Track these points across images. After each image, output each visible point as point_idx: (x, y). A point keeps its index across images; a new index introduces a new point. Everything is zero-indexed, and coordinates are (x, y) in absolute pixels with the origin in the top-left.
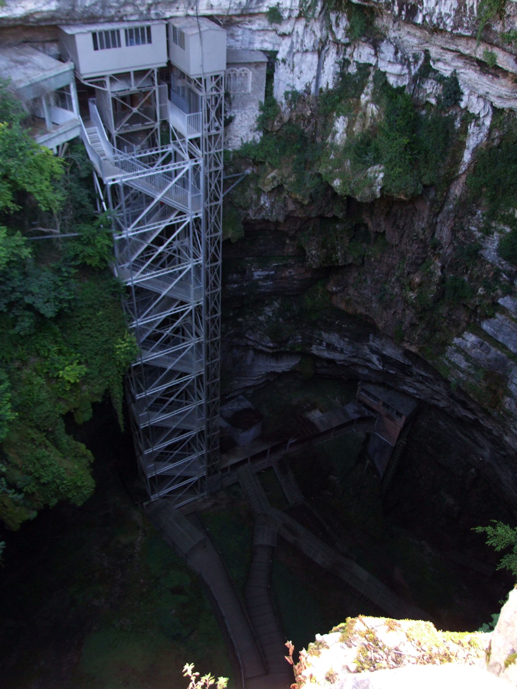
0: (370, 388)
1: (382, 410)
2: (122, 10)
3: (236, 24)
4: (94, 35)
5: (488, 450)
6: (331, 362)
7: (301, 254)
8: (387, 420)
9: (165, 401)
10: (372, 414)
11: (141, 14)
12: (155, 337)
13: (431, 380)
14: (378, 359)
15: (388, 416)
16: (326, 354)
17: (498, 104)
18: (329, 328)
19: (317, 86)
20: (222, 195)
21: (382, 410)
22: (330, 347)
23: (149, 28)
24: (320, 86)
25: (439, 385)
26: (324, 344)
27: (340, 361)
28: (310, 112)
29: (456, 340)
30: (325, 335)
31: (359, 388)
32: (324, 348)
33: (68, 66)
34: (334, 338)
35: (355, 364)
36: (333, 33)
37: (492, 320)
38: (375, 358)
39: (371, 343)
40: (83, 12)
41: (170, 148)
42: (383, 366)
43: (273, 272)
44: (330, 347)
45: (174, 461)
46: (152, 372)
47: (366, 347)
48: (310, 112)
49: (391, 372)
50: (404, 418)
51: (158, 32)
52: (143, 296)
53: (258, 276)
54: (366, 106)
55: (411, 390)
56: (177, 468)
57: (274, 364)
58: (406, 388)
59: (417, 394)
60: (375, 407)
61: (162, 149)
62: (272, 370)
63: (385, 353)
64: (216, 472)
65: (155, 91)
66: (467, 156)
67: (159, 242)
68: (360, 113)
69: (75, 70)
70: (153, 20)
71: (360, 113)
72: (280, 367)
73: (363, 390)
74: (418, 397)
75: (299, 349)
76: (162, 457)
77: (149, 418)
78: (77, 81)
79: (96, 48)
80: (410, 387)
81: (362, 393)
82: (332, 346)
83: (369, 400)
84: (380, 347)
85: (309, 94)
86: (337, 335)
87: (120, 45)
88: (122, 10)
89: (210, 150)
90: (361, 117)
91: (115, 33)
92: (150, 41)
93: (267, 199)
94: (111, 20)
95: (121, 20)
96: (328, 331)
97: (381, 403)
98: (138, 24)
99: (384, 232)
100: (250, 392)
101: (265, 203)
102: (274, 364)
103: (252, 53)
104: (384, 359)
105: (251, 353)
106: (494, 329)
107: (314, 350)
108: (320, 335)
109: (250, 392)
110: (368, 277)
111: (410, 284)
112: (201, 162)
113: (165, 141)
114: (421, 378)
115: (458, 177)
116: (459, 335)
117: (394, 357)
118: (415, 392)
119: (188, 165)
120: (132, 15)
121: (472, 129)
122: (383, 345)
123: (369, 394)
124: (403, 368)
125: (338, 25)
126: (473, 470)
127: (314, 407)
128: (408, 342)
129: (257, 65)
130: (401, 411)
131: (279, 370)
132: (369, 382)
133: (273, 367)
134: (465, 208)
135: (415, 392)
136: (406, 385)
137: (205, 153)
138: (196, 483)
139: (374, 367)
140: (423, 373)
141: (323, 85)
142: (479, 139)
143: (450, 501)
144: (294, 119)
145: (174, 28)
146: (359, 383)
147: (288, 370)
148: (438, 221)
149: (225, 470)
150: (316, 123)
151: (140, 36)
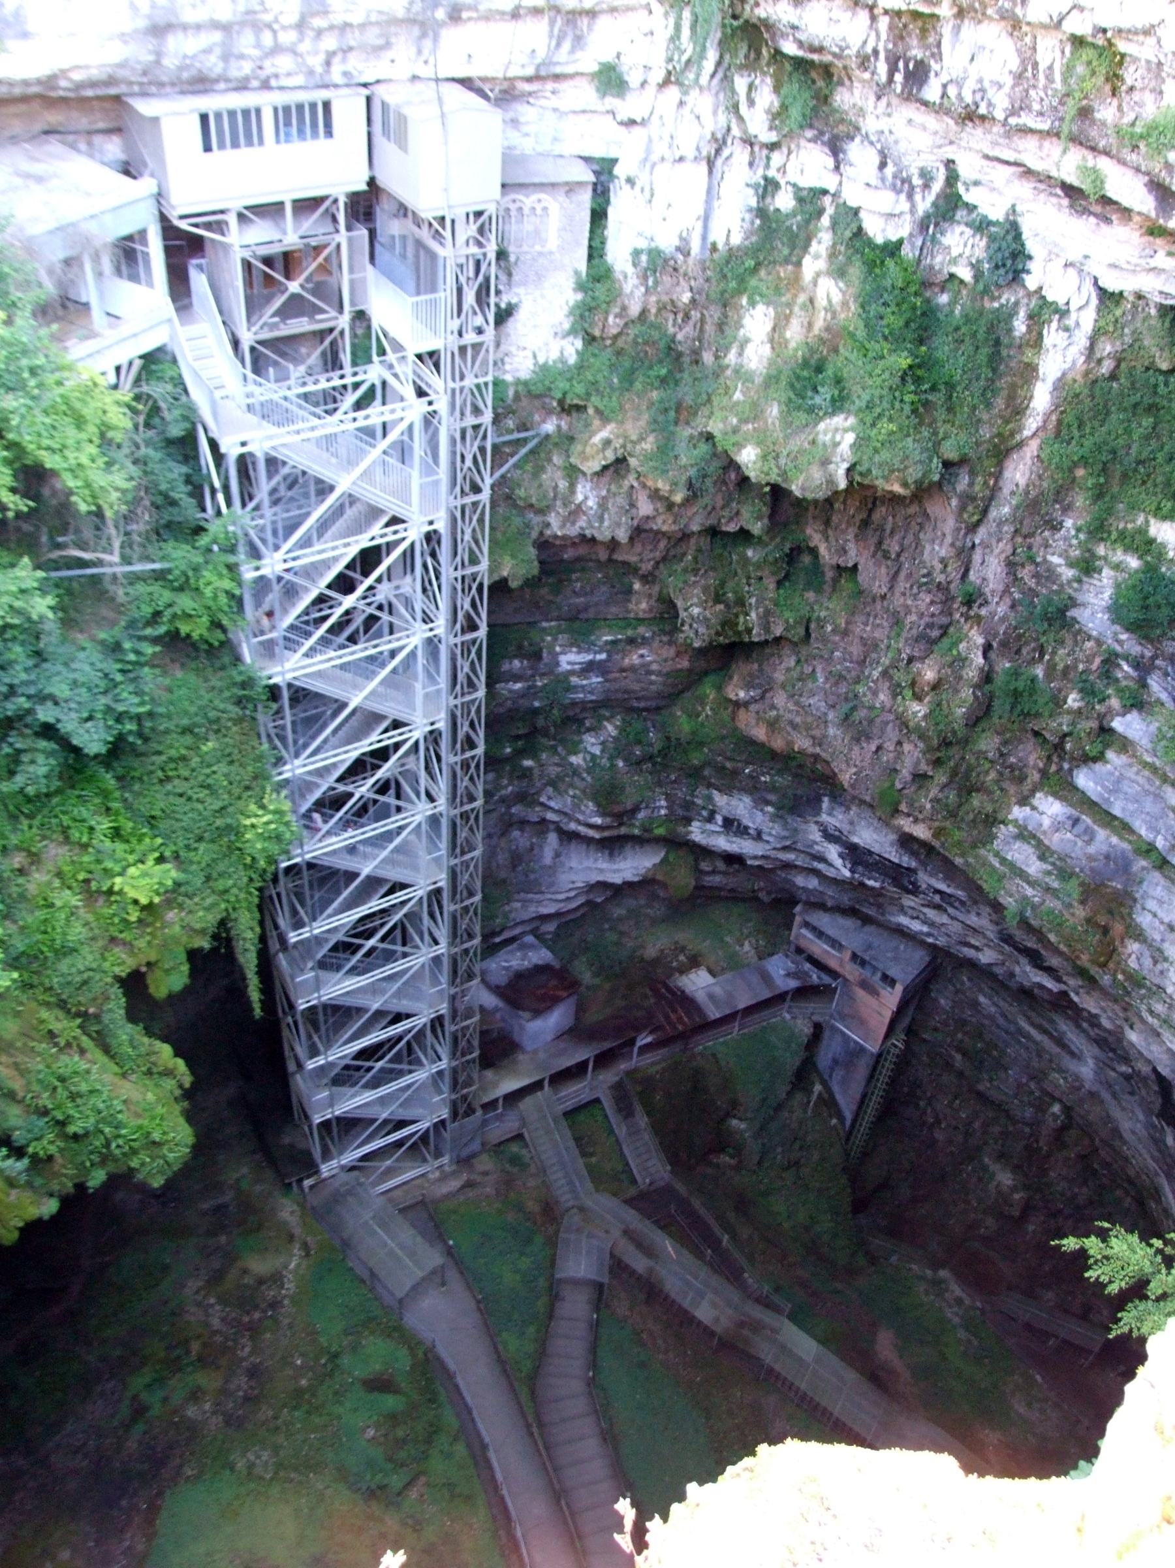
0: (823, 920)
1: (851, 971)
2: (267, 64)
3: (525, 97)
4: (204, 118)
5: (1091, 1062)
6: (734, 860)
7: (667, 615)
8: (860, 993)
9: (355, 949)
10: (827, 979)
11: (311, 72)
12: (332, 803)
13: (963, 903)
14: (841, 855)
15: (864, 985)
16: (723, 843)
17: (1112, 283)
18: (730, 782)
19: (704, 238)
20: (488, 481)
21: (851, 971)
22: (730, 824)
23: (327, 105)
24: (711, 239)
25: (978, 914)
26: (719, 819)
27: (755, 857)
28: (689, 295)
29: (1018, 813)
30: (720, 800)
31: (798, 919)
32: (718, 829)
33: (146, 186)
34: (740, 806)
35: (788, 866)
36: (741, 119)
37: (1098, 767)
38: (833, 852)
39: (824, 817)
40: (181, 68)
41: (373, 373)
42: (852, 871)
43: (603, 656)
44: (730, 824)
45: (375, 1084)
46: (325, 880)
47: (814, 828)
48: (689, 295)
49: (871, 883)
50: (899, 988)
51: (349, 112)
52: (308, 707)
53: (569, 663)
54: (815, 283)
55: (916, 926)
56: (382, 1101)
57: (603, 864)
58: (903, 920)
59: (929, 935)
60: (833, 964)
61: (355, 374)
62: (601, 878)
63: (855, 839)
64: (470, 1111)
65: (338, 246)
66: (1041, 398)
67: (344, 584)
68: (802, 298)
69: (160, 197)
70: (336, 86)
71: (802, 298)
72: (618, 871)
73: (806, 924)
74: (930, 940)
75: (660, 831)
76: (346, 1076)
77: (318, 985)
78: (164, 219)
79: (208, 148)
80: (913, 918)
81: (804, 931)
82: (739, 825)
83: (819, 948)
84: (845, 828)
85: (687, 254)
86: (747, 800)
87: (261, 142)
88: (267, 64)
89: (462, 378)
90: (803, 307)
91: (250, 116)
92: (329, 133)
93: (592, 489)
94: (242, 86)
95: (266, 85)
96: (727, 790)
97: (847, 955)
98: (304, 97)
99: (855, 566)
100: (550, 927)
101: (586, 498)
102: (605, 865)
103: (560, 161)
104: (855, 854)
105: (552, 837)
106: (1103, 786)
107: (697, 833)
108: (710, 798)
109: (550, 927)
110: (819, 669)
111: (913, 684)
112: (442, 405)
113: (361, 356)
114: (937, 898)
115: (1021, 445)
116: (1024, 801)
117: (876, 849)
118: (925, 929)
119: (416, 409)
120: (289, 74)
121: (1052, 336)
122: (852, 823)
123: (820, 934)
124: (898, 876)
125: (751, 103)
126: (1056, 1108)
127: (694, 962)
128: (908, 815)
129: (571, 188)
130: (891, 973)
131: (617, 879)
132: (822, 906)
133: (601, 871)
134: (1038, 512)
135: (925, 929)
136: (905, 914)
137: (451, 385)
138: (424, 1138)
139: (831, 873)
140: (942, 886)
141: (717, 236)
142: (1069, 359)
143: (1005, 1178)
144: (653, 311)
145: (384, 105)
146: (798, 909)
147: (636, 879)
148: (977, 541)
149: (490, 1106)
150: (703, 320)
151: (311, 119)
